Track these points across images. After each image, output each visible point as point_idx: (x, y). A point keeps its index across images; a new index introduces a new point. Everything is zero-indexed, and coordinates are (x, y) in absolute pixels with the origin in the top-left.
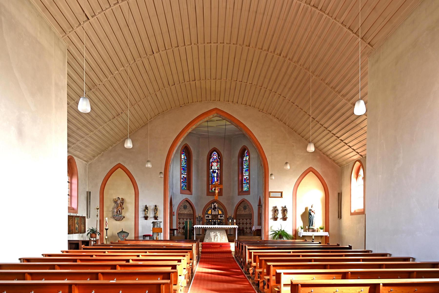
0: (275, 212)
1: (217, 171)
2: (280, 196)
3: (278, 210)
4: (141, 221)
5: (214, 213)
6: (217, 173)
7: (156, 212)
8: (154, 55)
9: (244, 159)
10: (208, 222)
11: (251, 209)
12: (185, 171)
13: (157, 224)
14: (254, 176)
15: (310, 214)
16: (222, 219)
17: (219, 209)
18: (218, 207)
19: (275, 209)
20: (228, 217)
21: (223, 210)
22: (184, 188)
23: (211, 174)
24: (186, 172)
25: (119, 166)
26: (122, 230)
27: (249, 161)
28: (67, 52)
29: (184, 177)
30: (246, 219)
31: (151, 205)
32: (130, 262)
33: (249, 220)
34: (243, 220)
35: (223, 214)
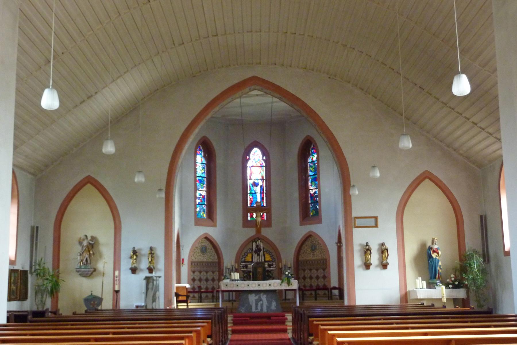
0: (365, 253)
1: (261, 183)
2: (374, 225)
3: (387, 250)
4: (126, 275)
5: (256, 259)
6: (261, 186)
7: (152, 260)
8: (150, 5)
10: (246, 276)
11: (325, 250)
12: (204, 184)
13: (153, 280)
15: (430, 256)
16: (271, 270)
17: (266, 253)
18: (264, 248)
19: (384, 248)
20: (280, 267)
21: (274, 254)
22: (202, 214)
23: (250, 189)
24: (205, 187)
25: (90, 181)
26: (92, 294)
27: (318, 163)
29: (201, 195)
30: (317, 270)
31: (143, 246)
33: (322, 271)
34: (311, 270)
35: (273, 260)
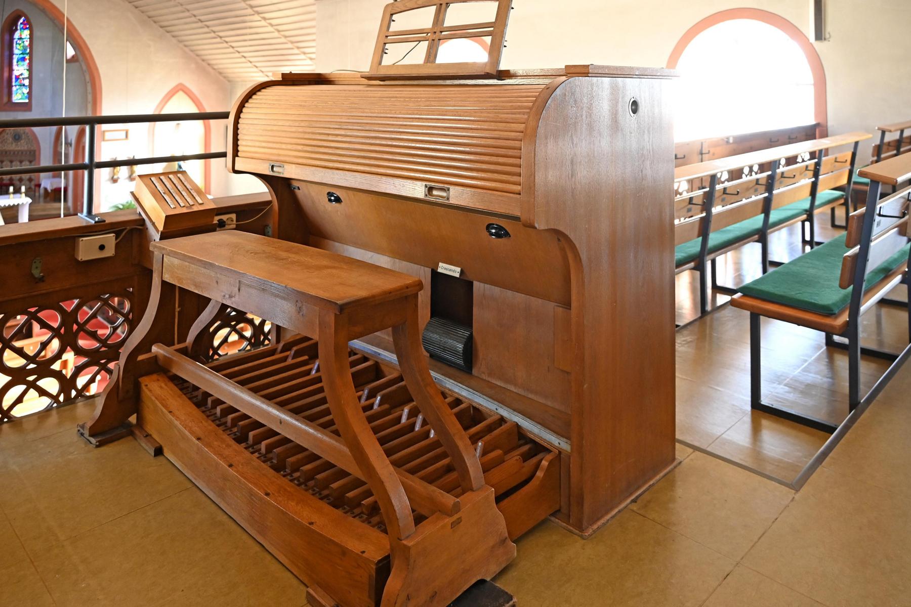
2: (124, 136)
9: (17, 35)
14: (41, 75)
28: (358, 341)
32: (153, 351)
